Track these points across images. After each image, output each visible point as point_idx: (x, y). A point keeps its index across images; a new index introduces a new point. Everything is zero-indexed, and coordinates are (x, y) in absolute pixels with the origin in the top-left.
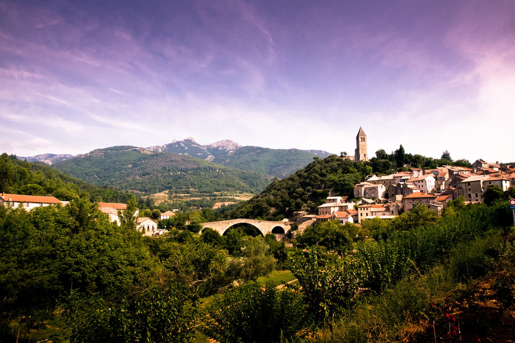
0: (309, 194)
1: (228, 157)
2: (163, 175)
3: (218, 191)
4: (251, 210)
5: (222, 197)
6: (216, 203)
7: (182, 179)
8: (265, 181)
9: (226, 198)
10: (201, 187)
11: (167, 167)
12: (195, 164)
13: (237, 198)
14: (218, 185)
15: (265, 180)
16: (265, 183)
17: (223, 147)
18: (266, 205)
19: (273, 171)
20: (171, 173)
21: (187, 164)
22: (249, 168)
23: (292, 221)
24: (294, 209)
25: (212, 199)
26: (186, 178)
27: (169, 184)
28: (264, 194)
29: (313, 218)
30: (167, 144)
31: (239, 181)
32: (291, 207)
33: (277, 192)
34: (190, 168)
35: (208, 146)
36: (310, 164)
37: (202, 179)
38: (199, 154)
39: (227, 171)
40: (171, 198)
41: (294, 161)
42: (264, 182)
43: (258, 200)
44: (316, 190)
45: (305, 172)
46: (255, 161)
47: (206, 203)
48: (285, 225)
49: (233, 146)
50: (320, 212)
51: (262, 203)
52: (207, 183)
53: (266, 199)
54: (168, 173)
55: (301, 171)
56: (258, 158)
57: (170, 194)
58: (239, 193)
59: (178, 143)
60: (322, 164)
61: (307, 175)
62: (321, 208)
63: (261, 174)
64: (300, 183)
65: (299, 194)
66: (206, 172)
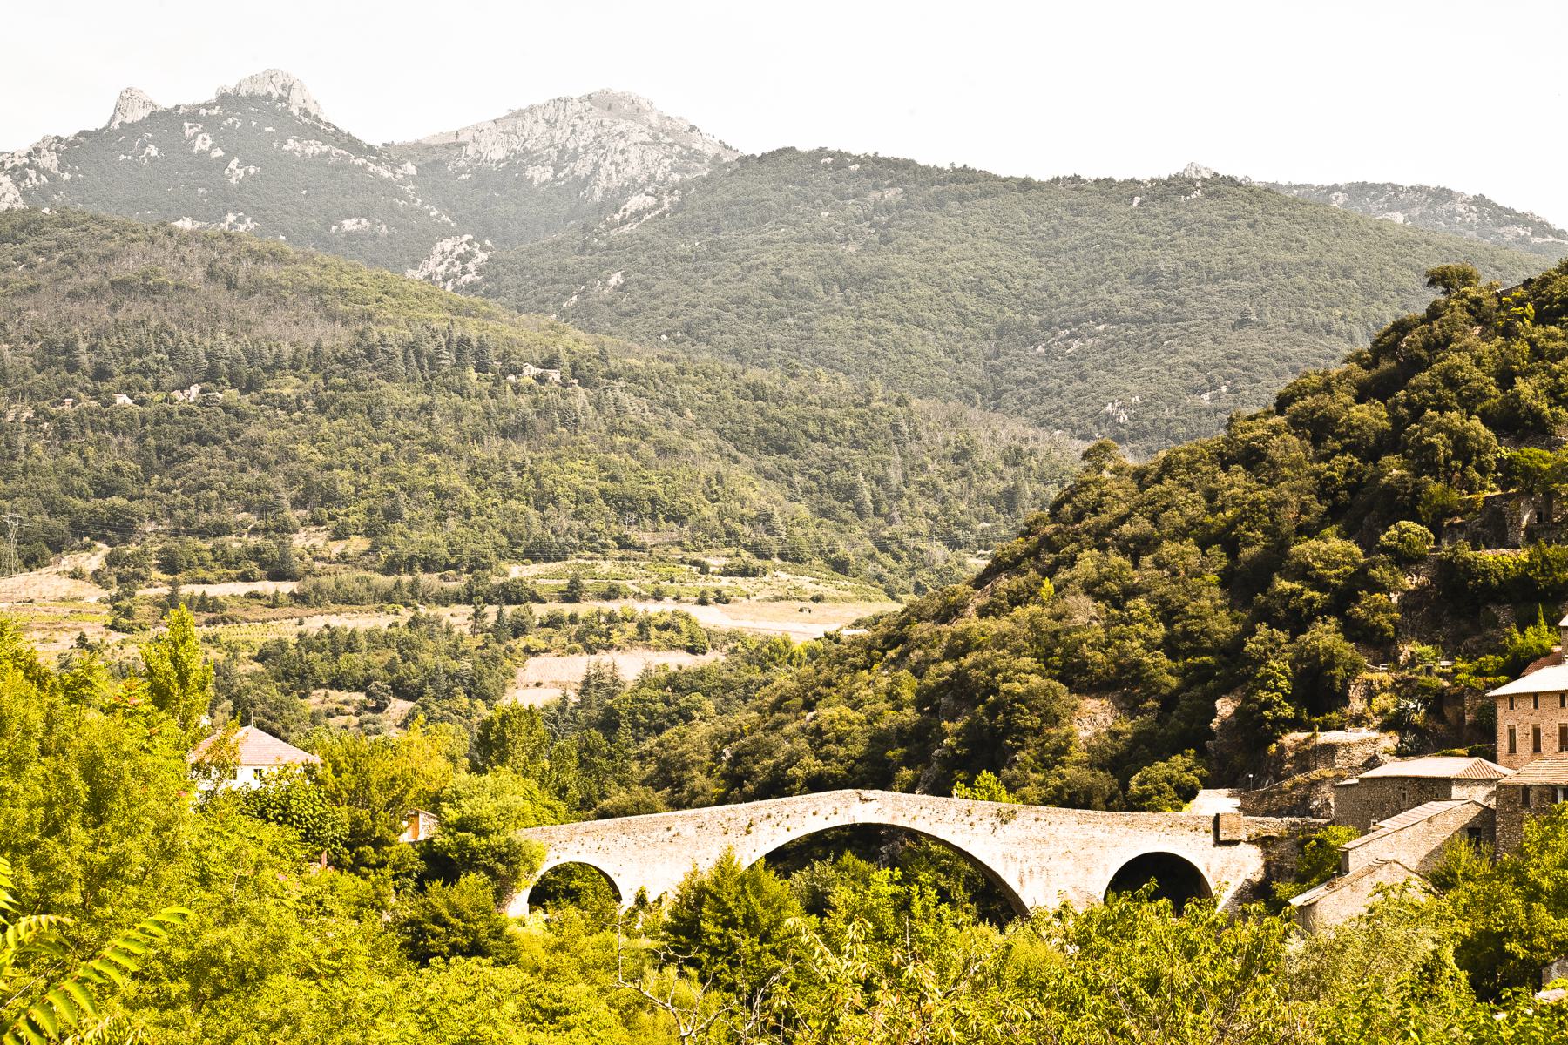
0: (1410, 582)
1: (617, 253)
2: (50, 418)
3: (540, 552)
4: (909, 715)
5: (583, 609)
6: (532, 661)
7: (218, 449)
8: (950, 467)
9: (611, 618)
10: (392, 515)
11: (82, 345)
12: (332, 317)
13: (710, 618)
14: (544, 500)
15: (956, 459)
16: (955, 487)
17: (566, 156)
18: (1035, 680)
19: (1021, 373)
20: (122, 400)
21: (253, 315)
22: (807, 349)
23: (1268, 813)
24: (1289, 711)
25: (491, 620)
26: (257, 443)
27: (105, 489)
28: (1003, 583)
29: (1461, 781)
30: (68, 132)
31: (720, 465)
32: (1262, 694)
33: (1128, 563)
34: (287, 350)
35: (429, 148)
36: (1401, 327)
37: (398, 447)
38: (349, 225)
39: (615, 376)
40: (128, 613)
41: (1209, 288)
42: (948, 478)
43: (963, 636)
44: (1470, 554)
45: (1360, 399)
46: (854, 281)
47: (440, 661)
48: (1218, 843)
49: (652, 155)
50: (1512, 732)
51: (1001, 658)
52: (442, 480)
53: (1034, 627)
54: (95, 394)
55: (1327, 388)
56: (879, 261)
57: (121, 580)
58: (726, 573)
59: (166, 121)
60: (1508, 332)
61: (1387, 425)
62: (1520, 704)
63: (915, 403)
64: (1324, 489)
65: (1320, 584)
66: (428, 387)
